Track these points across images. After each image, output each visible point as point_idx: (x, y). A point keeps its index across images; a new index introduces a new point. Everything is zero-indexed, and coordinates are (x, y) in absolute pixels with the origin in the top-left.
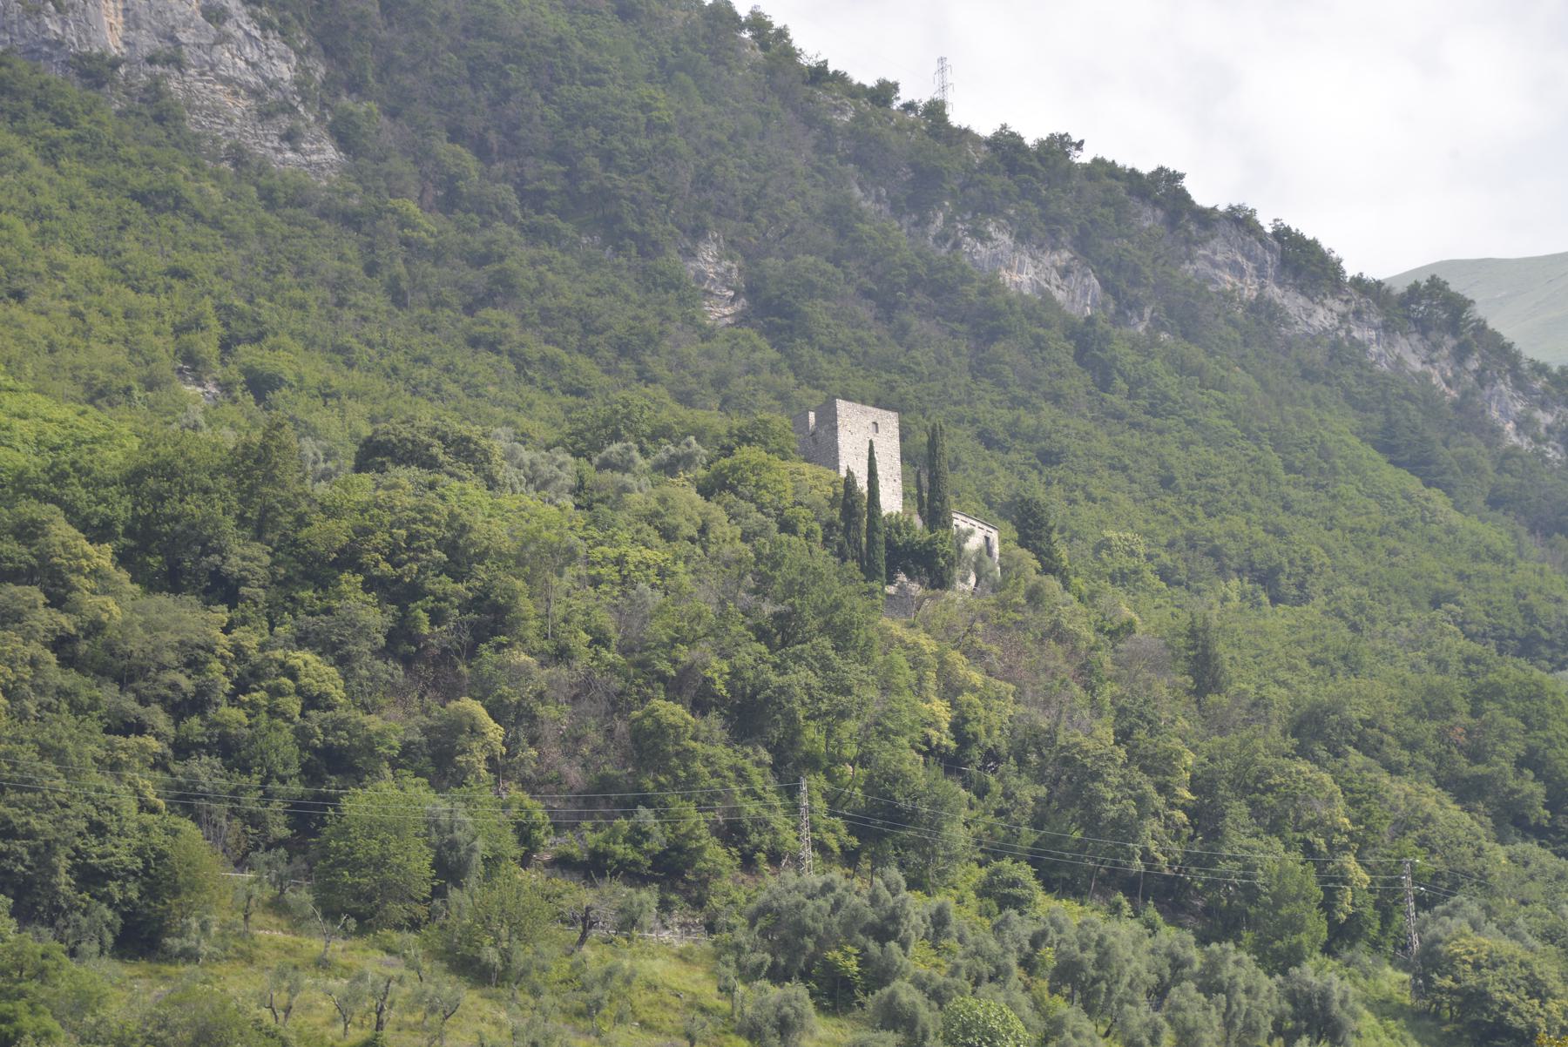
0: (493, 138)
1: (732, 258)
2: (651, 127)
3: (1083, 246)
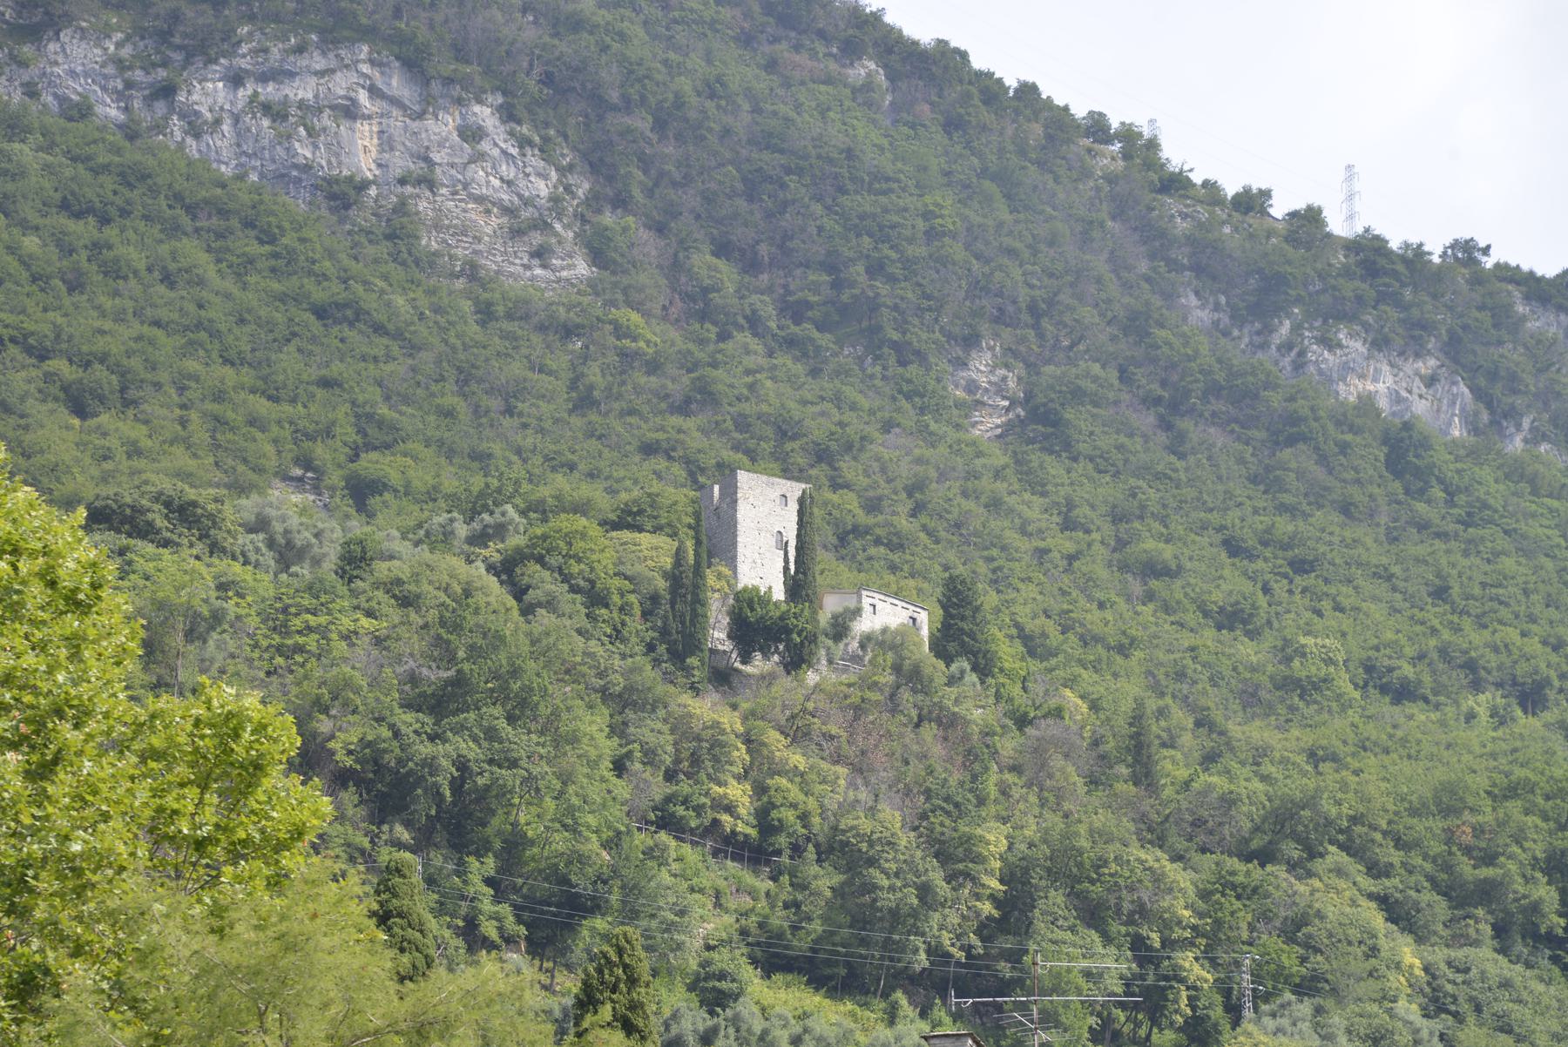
0: (764, 250)
1: (1007, 366)
2: (931, 235)
3: (1454, 350)
